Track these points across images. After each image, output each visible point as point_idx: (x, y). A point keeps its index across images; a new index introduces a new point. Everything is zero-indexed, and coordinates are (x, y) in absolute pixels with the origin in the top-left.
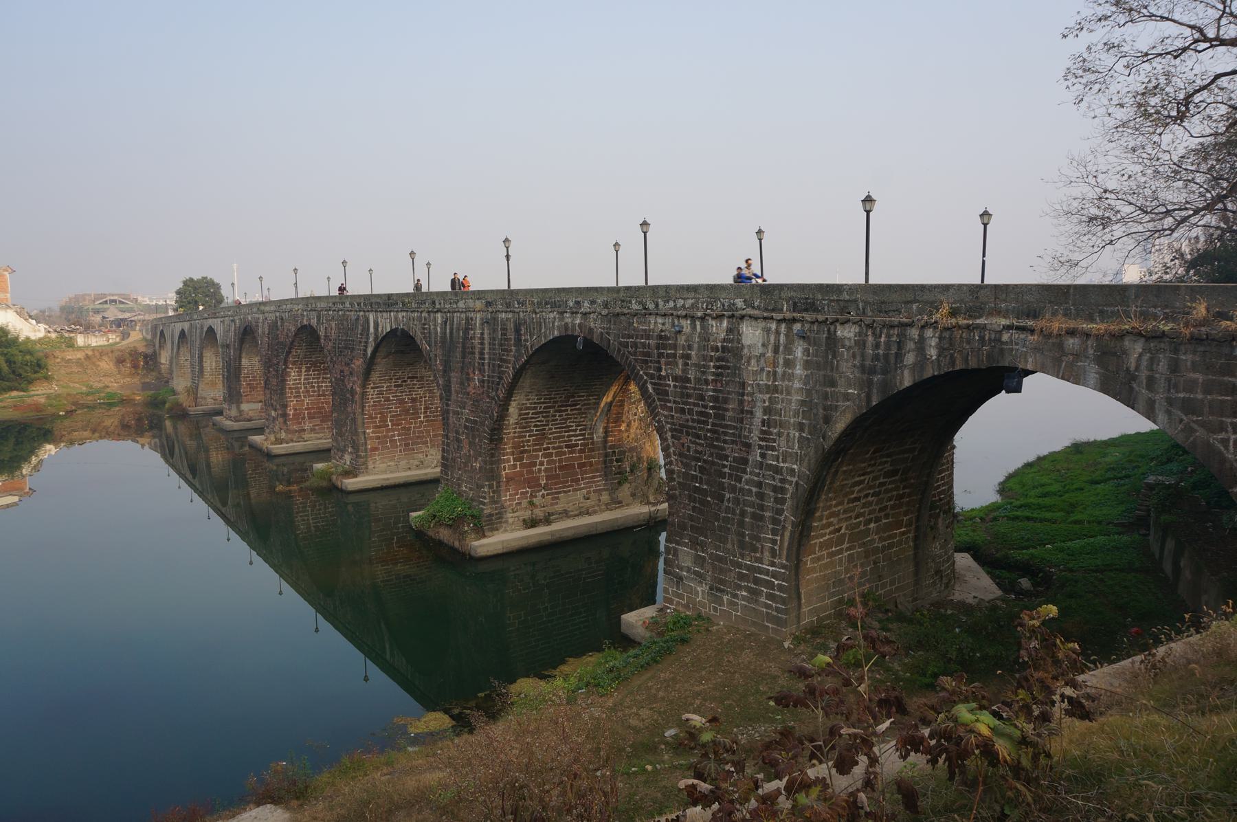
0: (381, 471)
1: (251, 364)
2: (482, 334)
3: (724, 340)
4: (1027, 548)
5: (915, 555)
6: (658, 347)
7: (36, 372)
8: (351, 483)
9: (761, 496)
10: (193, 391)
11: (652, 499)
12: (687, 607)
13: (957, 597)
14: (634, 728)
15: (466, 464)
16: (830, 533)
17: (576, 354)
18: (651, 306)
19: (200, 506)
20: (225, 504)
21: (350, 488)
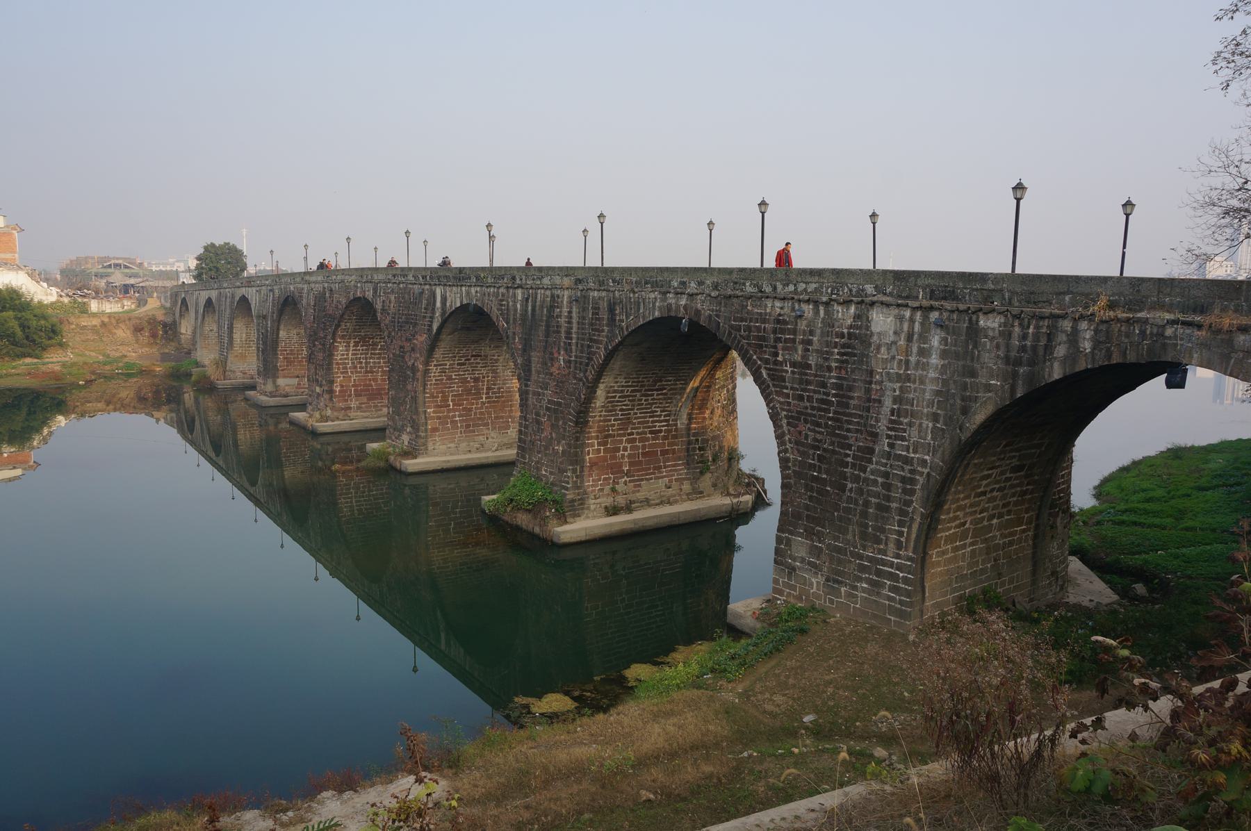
0: (441, 452)
1: (290, 336)
2: (570, 312)
3: (851, 327)
4: (1139, 553)
5: (1034, 554)
6: (775, 331)
7: (50, 338)
8: (411, 465)
9: (887, 487)
10: (222, 363)
11: (731, 491)
12: (799, 598)
13: (1072, 599)
14: (771, 713)
15: (546, 448)
16: (956, 527)
17: (671, 335)
18: (768, 289)
19: (223, 484)
20: (253, 484)
21: (410, 469)
